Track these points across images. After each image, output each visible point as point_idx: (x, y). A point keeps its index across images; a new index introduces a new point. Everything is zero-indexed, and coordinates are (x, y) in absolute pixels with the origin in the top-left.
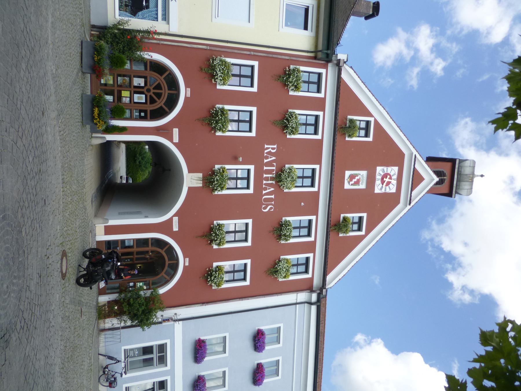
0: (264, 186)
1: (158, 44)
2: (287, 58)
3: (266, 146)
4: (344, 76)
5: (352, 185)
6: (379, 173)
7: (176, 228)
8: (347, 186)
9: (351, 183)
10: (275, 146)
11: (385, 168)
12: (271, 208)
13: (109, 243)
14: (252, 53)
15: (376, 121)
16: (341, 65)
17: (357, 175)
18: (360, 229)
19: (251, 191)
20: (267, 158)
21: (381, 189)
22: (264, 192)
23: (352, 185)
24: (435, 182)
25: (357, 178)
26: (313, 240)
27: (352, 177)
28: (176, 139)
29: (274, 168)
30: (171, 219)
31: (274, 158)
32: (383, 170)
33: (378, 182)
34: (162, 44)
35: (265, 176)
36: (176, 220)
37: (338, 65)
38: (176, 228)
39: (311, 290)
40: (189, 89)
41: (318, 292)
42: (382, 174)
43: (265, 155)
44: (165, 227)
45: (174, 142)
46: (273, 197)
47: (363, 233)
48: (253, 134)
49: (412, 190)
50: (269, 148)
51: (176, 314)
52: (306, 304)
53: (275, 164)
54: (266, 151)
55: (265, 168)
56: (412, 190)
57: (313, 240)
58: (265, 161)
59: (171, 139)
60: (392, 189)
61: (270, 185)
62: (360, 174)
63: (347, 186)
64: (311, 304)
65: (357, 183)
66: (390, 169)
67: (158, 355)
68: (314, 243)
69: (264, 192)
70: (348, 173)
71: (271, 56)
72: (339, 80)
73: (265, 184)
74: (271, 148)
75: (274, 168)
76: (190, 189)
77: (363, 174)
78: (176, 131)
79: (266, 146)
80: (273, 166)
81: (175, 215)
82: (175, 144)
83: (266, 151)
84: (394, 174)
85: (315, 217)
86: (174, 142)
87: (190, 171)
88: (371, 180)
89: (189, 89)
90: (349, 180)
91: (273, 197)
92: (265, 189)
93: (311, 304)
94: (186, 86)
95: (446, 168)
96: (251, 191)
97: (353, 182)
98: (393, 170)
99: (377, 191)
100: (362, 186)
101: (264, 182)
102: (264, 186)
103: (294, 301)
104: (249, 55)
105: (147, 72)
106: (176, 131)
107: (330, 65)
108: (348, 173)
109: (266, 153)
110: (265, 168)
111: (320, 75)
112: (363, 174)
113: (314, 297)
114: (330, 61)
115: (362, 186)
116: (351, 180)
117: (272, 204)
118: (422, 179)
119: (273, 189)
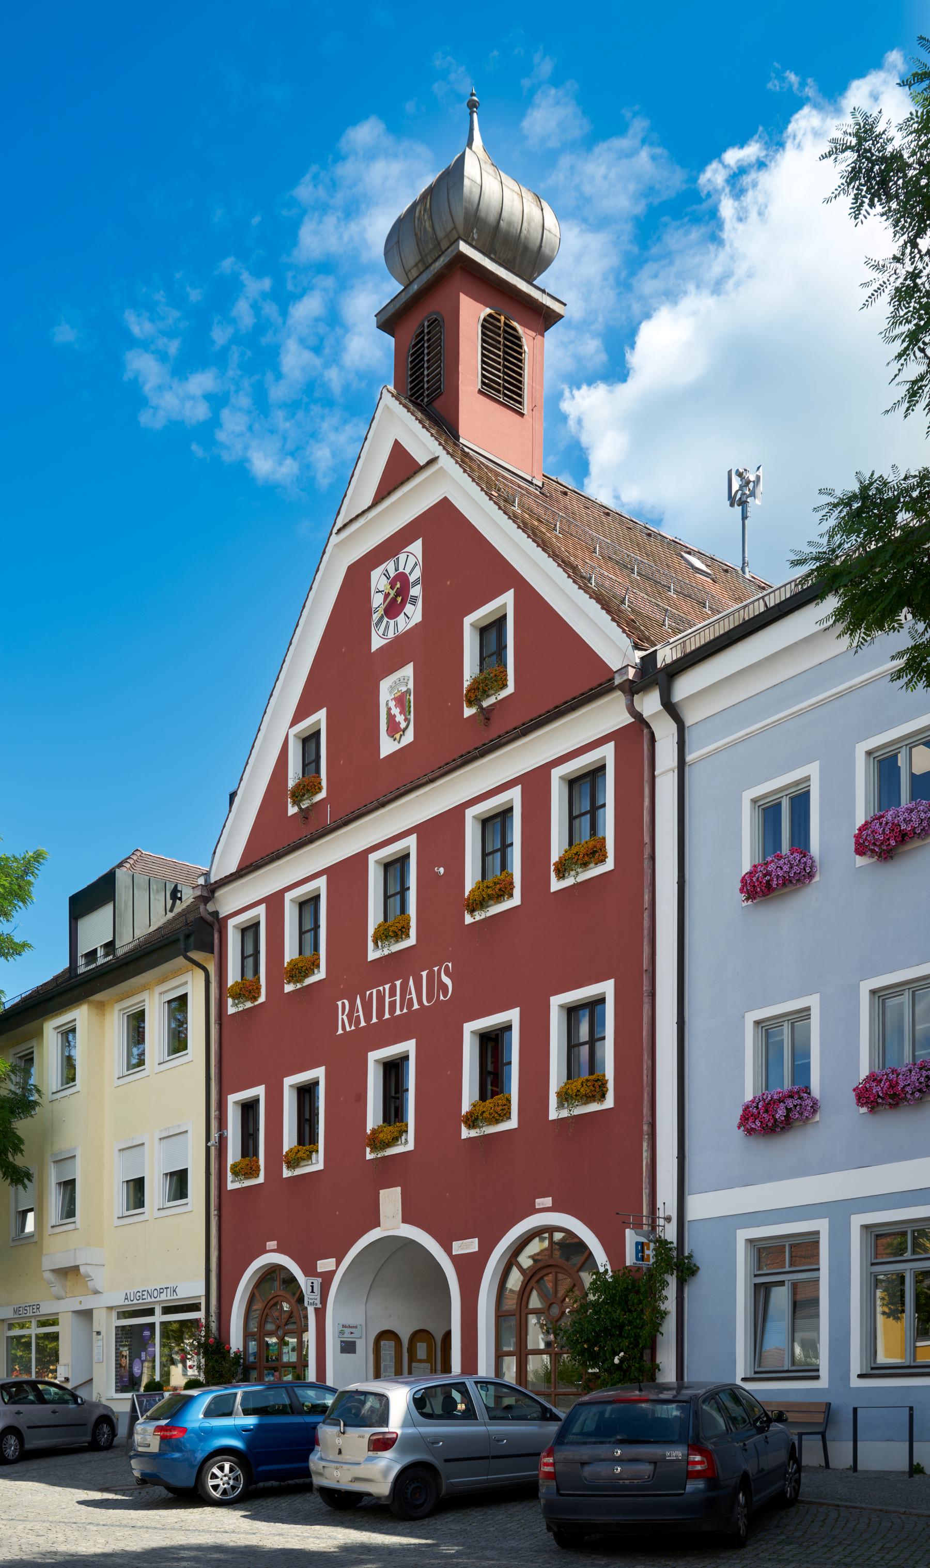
3: (340, 1031)
10: (340, 1003)
50: (343, 1019)
81: (448, 1250)
87: (377, 1224)
117: (439, 971)
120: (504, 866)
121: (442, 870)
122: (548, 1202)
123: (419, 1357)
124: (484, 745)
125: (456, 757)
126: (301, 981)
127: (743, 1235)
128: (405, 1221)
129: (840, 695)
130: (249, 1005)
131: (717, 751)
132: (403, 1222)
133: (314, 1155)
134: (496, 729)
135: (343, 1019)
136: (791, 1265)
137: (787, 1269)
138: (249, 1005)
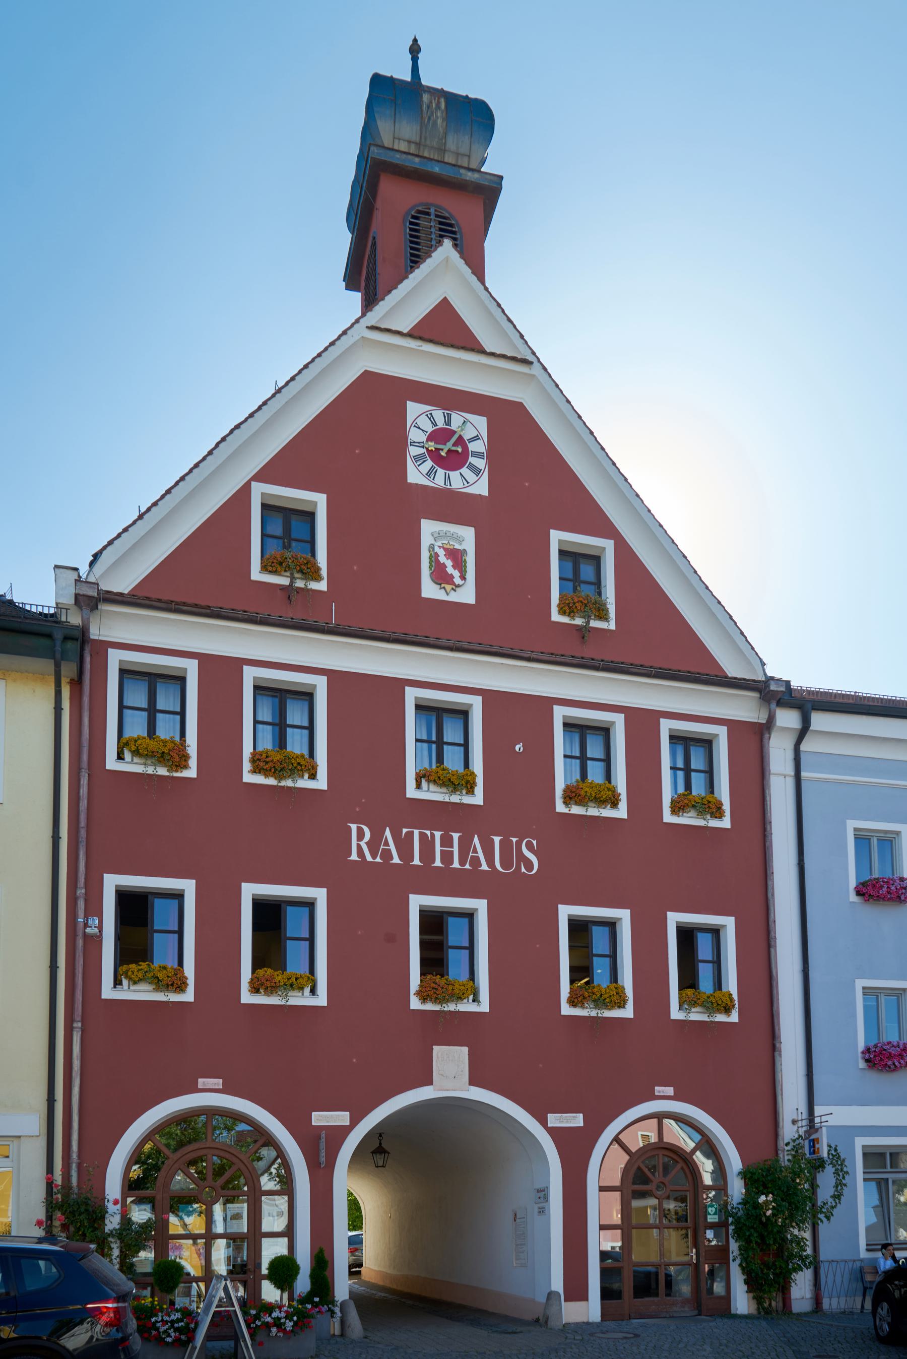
0: (467, 867)
1: (79, 1166)
2: (84, 781)
3: (354, 857)
4: (124, 584)
5: (463, 578)
6: (428, 474)
7: (577, 1120)
8: (467, 594)
9: (457, 580)
10: (354, 827)
11: (414, 451)
12: (530, 847)
13: (607, 1294)
14: (81, 892)
15: (262, 476)
16: (95, 594)
17: (434, 558)
18: (596, 560)
19: (481, 906)
20: (387, 855)
21: (477, 471)
22: (484, 867)
23: (463, 578)
24: (455, 255)
25: (442, 559)
26: (479, 699)
27: (441, 577)
28: (341, 1118)
29: (416, 833)
30: (555, 1133)
31: (388, 833)
32: (416, 458)
33: (457, 480)
34: (79, 1156)
35: (438, 863)
36: (554, 1120)
37: (92, 599)
38: (577, 1120)
39: (763, 730)
40: (201, 1081)
41: (773, 705)
42: (429, 463)
43: (378, 860)
44: (575, 1150)
45: (348, 1123)
46: (497, 840)
47: (608, 545)
48: (320, 895)
49: (483, 352)
50: (359, 848)
51: (794, 1122)
52: (804, 747)
53: (405, 831)
54: (369, 858)
55: (417, 861)
56: (483, 352)
57: (479, 699)
58: (396, 860)
59: (342, 1133)
60: (474, 428)
61: (465, 846)
62: (432, 547)
63: (467, 594)
64: (804, 730)
65: (457, 557)
66: (414, 435)
67: (889, 1169)
68: (206, 661)
69: (484, 867)
70: (430, 590)
71: (83, 833)
72: (140, 599)
73: (462, 863)
74: (359, 842)
75: (416, 833)
76: (474, 1080)
77: (431, 532)
78: (319, 1118)
79: (354, 857)
80: (410, 835)
81: (543, 1122)
82: (355, 1121)
83: (369, 858)
84: (431, 417)
85: (663, 721)
86: (348, 1123)
87: (427, 1080)
88: (451, 506)
89: (201, 1081)
90: (448, 587)
91: (497, 840)
92: (476, 862)
93: (804, 730)
94: (194, 1089)
95: (398, 199)
96: (481, 906)
97: (456, 574)
98: (420, 419)
99: (481, 487)
100: (466, 537)
101: (456, 865)
102: (467, 867)
103: (790, 783)
104: (86, 901)
105: (159, 1197)
106: (319, 1118)
107: (95, 633)
108: (430, 590)
109: (374, 857)
110: (417, 861)
111: (125, 673)
112: (431, 532)
113: (787, 719)
114: (80, 637)
115: (466, 537)
116: (449, 579)
117: (519, 844)
118: (444, 308)
119: (476, 840)
120: (608, 776)
121: (518, 747)
122: (670, 1091)
123: (284, 1252)
124: (593, 659)
125: (646, 664)
126: (280, 779)
127: (860, 1142)
128: (472, 1082)
129: (848, 783)
130: (162, 771)
131: (826, 781)
132: (470, 1084)
133: (151, 987)
134: (589, 651)
135: (359, 848)
136: (891, 1167)
137: (889, 1169)
138: (162, 771)
